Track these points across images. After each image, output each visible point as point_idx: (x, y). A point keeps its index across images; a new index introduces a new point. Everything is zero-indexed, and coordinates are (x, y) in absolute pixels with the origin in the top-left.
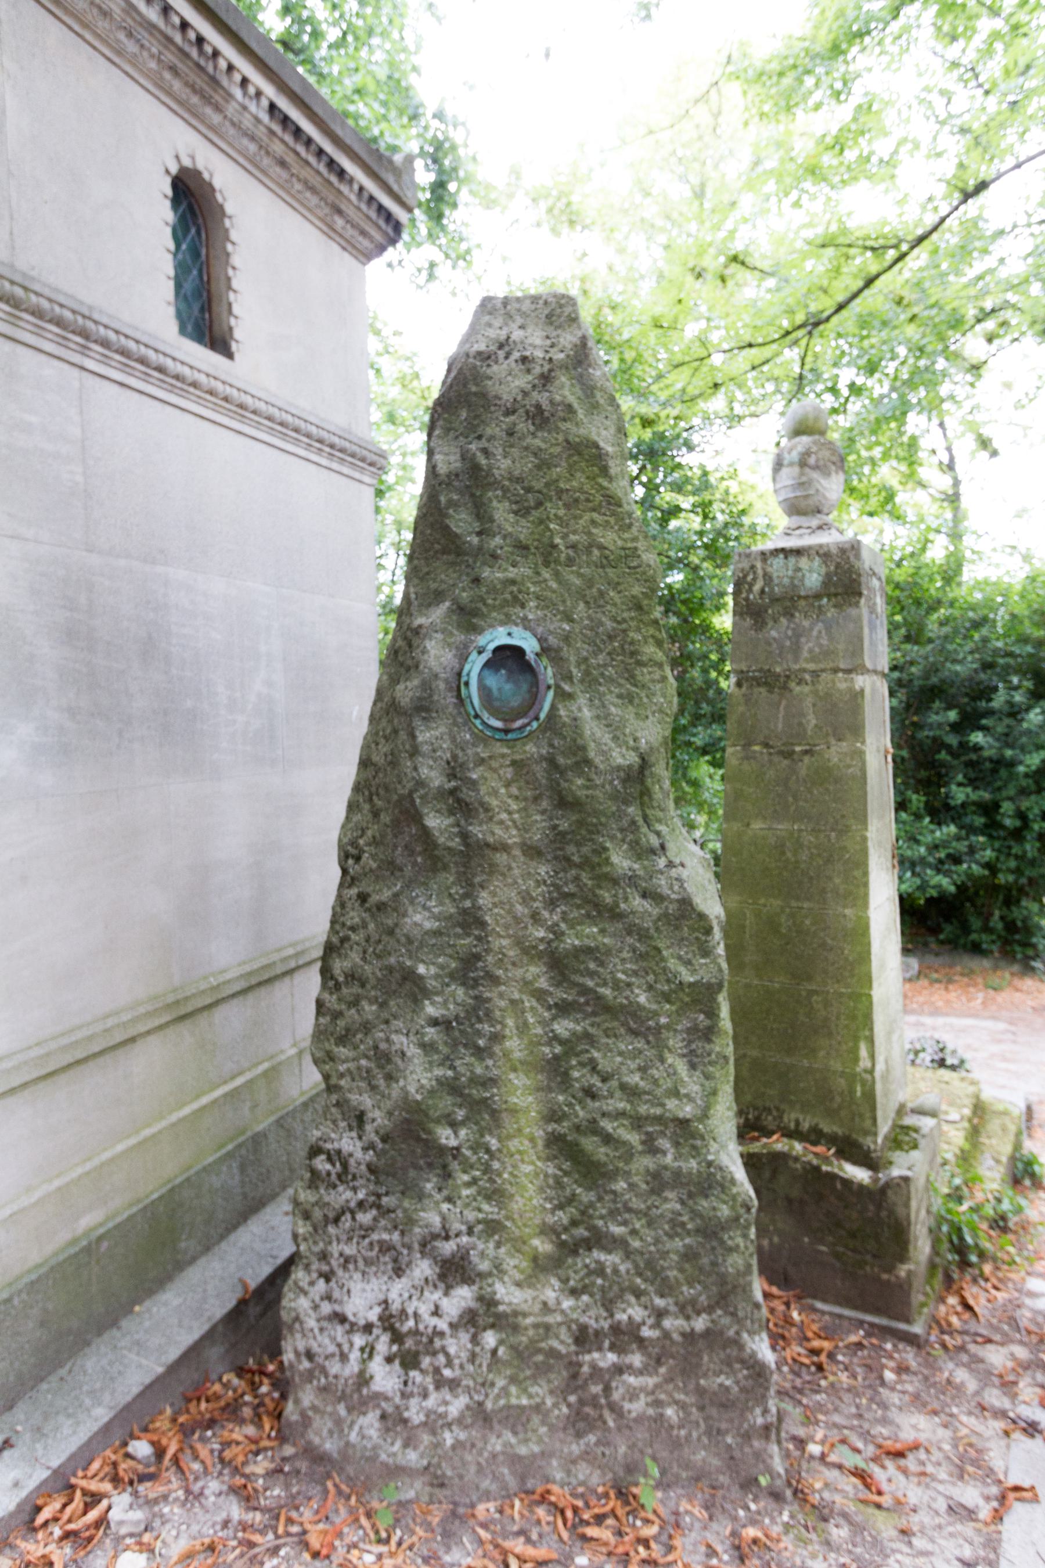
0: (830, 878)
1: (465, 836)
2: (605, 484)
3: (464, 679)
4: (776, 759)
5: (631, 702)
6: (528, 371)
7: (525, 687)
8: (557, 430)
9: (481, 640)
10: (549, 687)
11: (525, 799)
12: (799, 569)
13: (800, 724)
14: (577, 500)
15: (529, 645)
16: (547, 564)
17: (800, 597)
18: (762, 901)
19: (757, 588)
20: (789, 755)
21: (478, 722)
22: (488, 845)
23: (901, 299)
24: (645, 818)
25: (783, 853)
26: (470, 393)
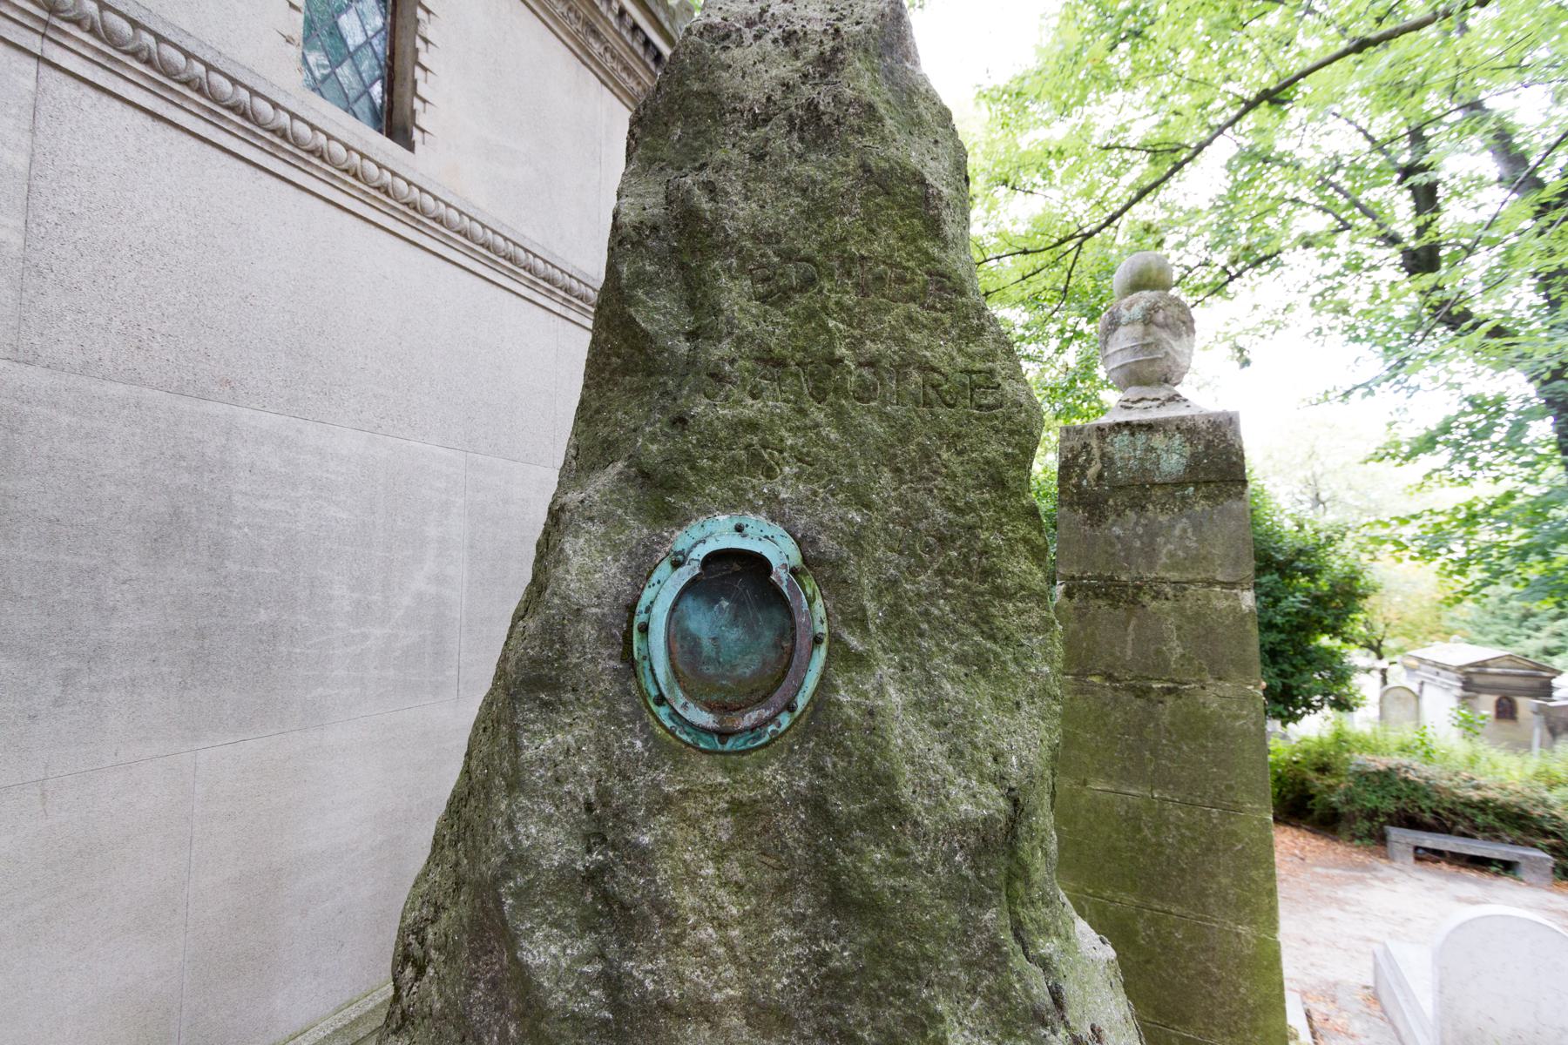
0: (1212, 876)
1: (613, 983)
2: (935, 252)
3: (639, 619)
4: (1125, 697)
5: (983, 671)
6: (796, 55)
7: (768, 636)
8: (847, 148)
9: (682, 540)
10: (817, 640)
11: (758, 891)
12: (1153, 449)
13: (1158, 652)
14: (880, 278)
15: (780, 551)
16: (819, 395)
17: (1153, 485)
18: (1108, 893)
19: (1092, 471)
20: (1144, 693)
21: (662, 712)
22: (666, 1007)
23: (1150, 226)
24: (1018, 930)
25: (1139, 830)
26: (690, 93)
